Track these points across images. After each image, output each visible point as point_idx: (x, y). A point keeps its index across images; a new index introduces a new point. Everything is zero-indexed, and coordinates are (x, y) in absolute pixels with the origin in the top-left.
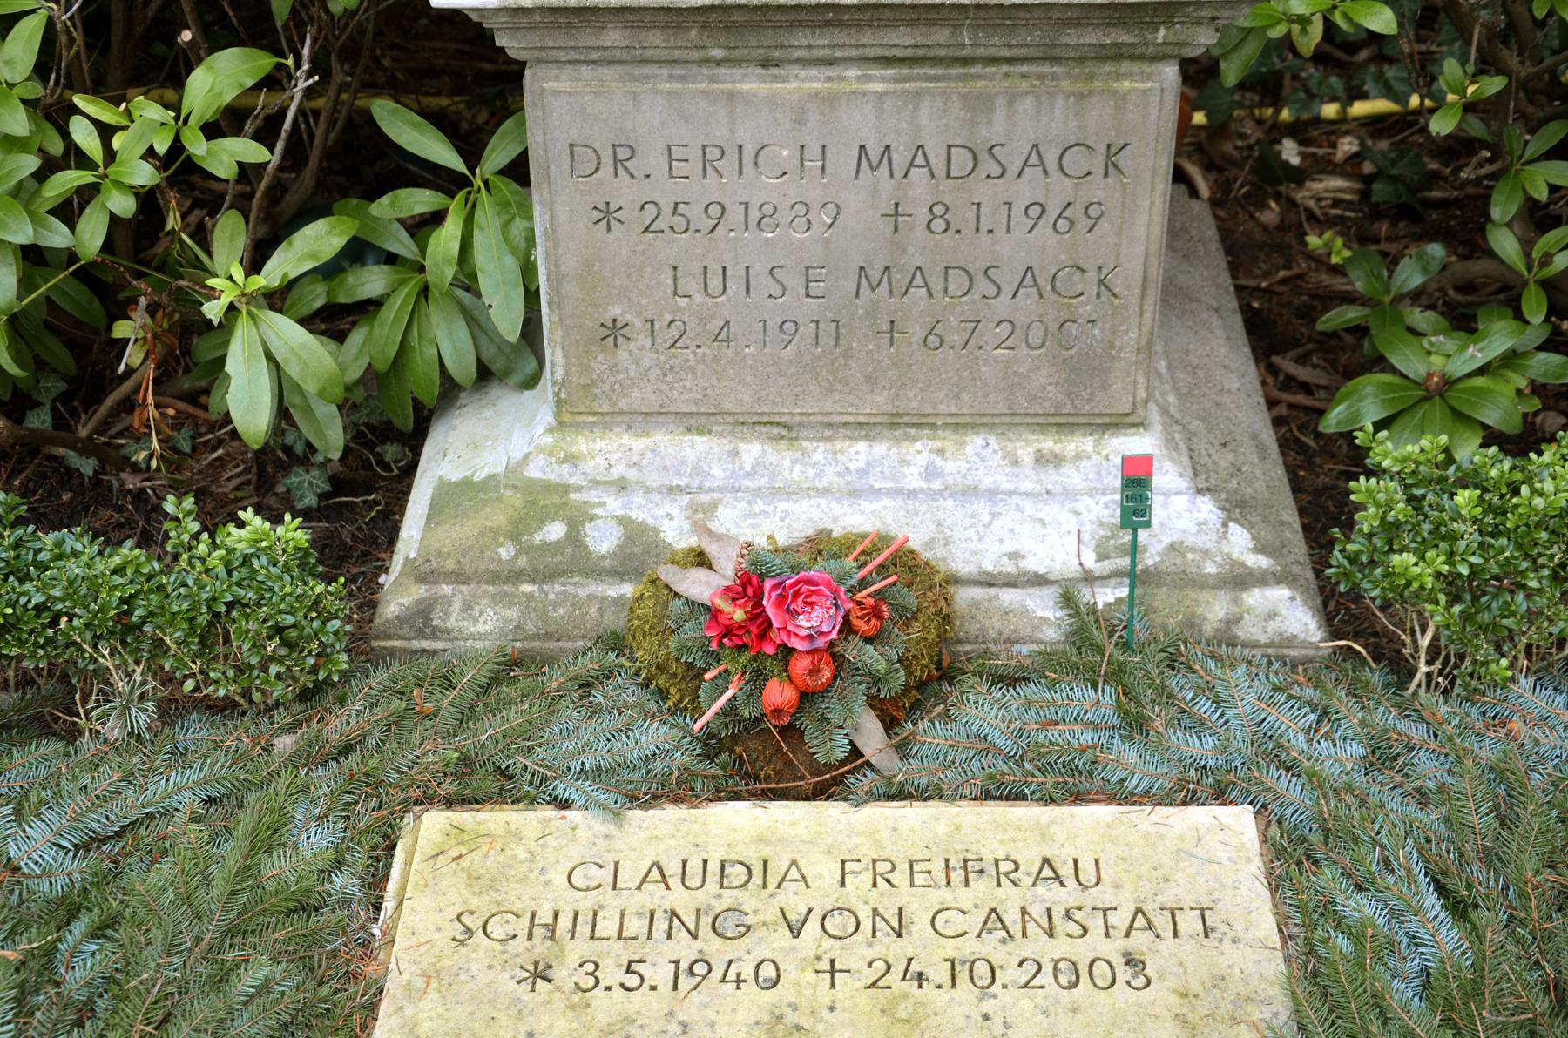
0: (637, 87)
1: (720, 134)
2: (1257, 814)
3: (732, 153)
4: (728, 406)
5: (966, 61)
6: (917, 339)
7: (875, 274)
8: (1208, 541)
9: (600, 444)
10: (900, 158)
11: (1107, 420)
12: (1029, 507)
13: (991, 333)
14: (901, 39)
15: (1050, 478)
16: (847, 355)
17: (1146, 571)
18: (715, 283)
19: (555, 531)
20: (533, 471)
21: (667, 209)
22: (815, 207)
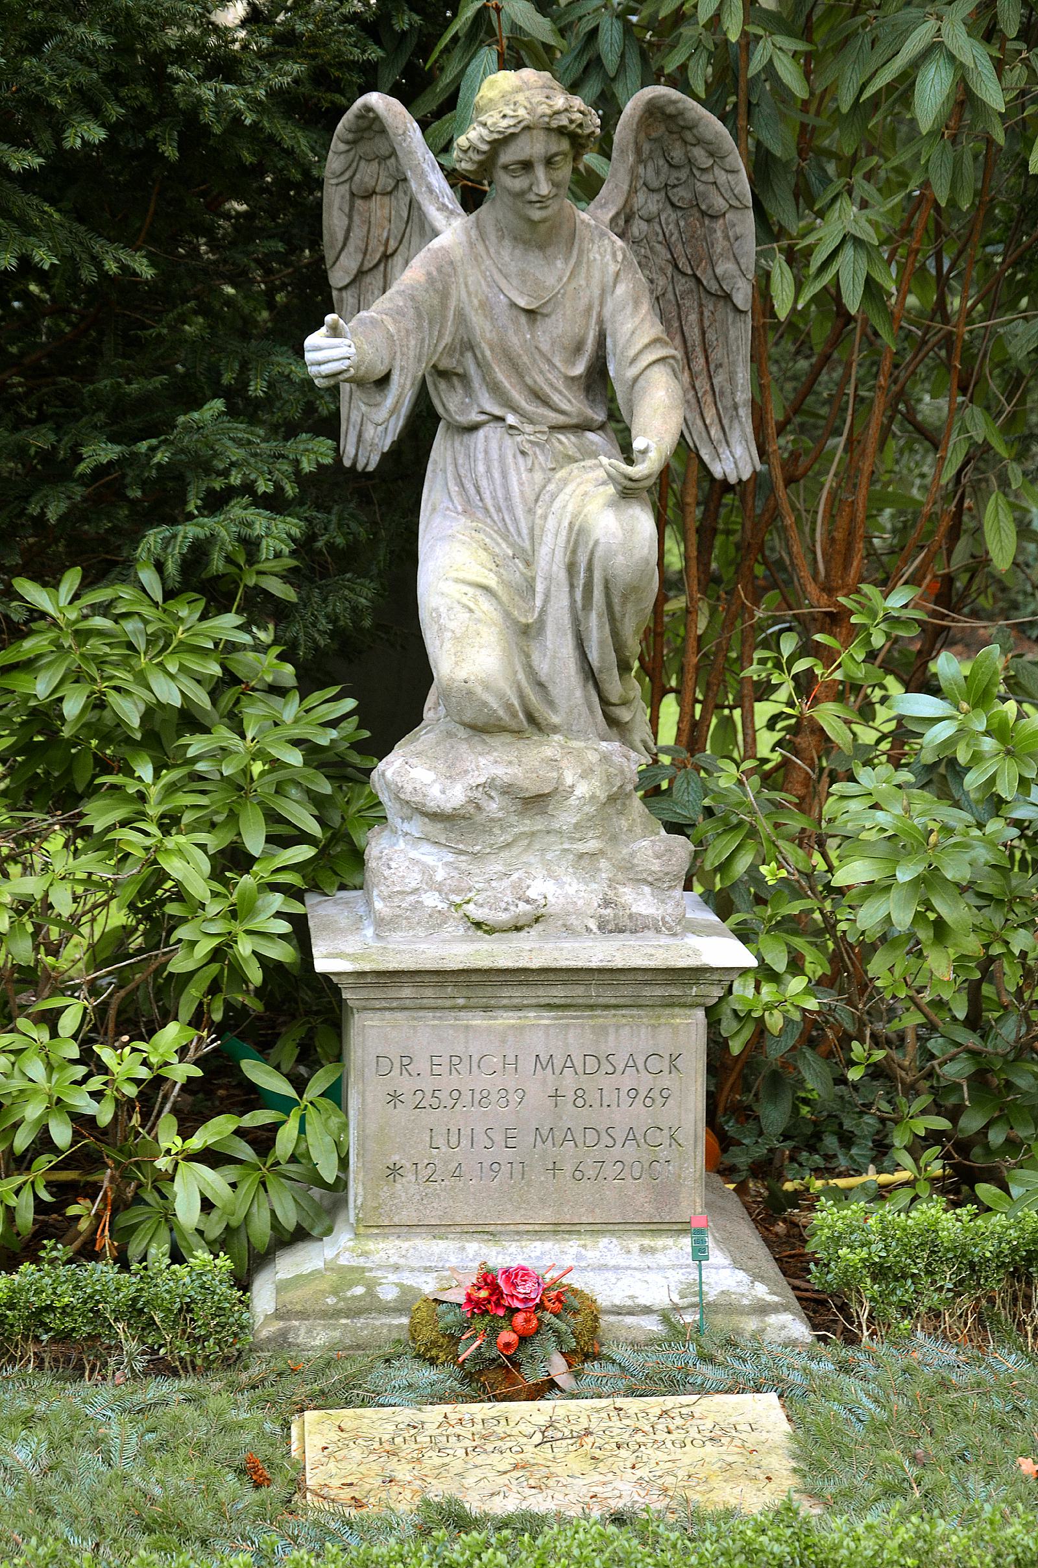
0: (415, 1023)
1: (459, 1050)
2: (780, 1397)
3: (466, 1060)
4: (458, 1220)
5: (592, 1007)
6: (568, 1174)
7: (545, 1132)
8: (744, 1289)
9: (382, 1245)
10: (558, 1062)
11: (680, 1227)
12: (637, 1274)
13: (610, 1170)
14: (558, 993)
15: (648, 1260)
16: (529, 1185)
17: (708, 1304)
18: (454, 1140)
19: (359, 1290)
20: (343, 1261)
21: (429, 1094)
22: (511, 1091)
